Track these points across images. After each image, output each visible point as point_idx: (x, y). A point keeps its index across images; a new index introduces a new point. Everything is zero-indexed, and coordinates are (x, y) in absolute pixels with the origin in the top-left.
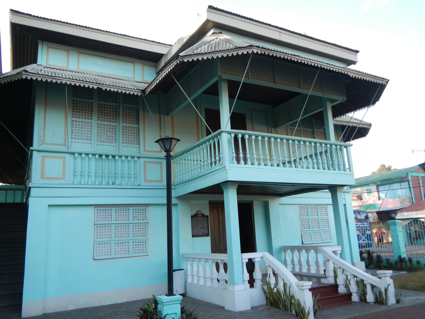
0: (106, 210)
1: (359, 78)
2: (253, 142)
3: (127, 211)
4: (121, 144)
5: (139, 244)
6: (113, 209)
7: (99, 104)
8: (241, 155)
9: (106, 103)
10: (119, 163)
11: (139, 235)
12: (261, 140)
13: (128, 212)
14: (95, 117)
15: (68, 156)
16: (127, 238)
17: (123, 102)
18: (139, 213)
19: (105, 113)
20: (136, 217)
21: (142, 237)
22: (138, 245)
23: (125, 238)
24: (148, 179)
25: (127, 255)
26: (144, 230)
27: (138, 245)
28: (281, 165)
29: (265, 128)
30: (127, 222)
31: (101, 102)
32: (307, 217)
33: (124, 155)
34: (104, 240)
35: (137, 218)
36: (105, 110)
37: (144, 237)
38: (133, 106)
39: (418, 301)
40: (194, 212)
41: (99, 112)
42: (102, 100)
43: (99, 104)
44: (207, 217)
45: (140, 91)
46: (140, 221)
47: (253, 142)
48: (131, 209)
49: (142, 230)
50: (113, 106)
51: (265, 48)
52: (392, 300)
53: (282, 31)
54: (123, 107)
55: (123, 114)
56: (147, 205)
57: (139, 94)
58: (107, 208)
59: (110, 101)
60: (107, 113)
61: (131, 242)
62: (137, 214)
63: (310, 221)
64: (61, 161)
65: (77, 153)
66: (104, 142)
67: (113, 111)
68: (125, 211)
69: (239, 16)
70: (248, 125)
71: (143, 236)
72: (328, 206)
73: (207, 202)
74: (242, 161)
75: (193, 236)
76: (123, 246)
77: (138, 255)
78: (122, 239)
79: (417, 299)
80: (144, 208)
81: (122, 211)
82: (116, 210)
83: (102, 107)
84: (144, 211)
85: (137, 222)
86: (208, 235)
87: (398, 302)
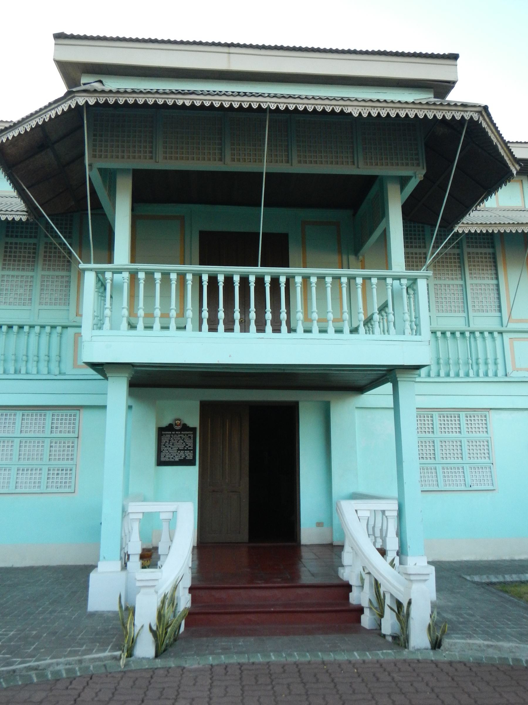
0: (6, 415)
1: (365, 115)
2: (158, 286)
3: (43, 417)
5: (60, 472)
6: (19, 413)
7: (7, 243)
8: (269, 316)
9: (19, 240)
10: (33, 338)
11: (61, 457)
12: (162, 280)
13: (44, 419)
14: (40, 267)
16: (39, 462)
17: (468, 246)
18: (64, 421)
19: (15, 257)
20: (57, 428)
21: (65, 462)
22: (58, 474)
23: (35, 462)
25: (36, 490)
26: (70, 449)
27: (58, 474)
28: (362, 329)
29: (335, 258)
30: (41, 435)
31: (9, 240)
32: (431, 435)
33: (18, 323)
34: (480, 461)
35: (59, 430)
36: (15, 252)
37: (70, 462)
38: (483, 250)
39: (490, 650)
40: (165, 423)
41: (5, 256)
42: (473, 247)
43: (7, 243)
44: (194, 429)
45: (25, 213)
46: (63, 435)
47: (158, 286)
48: (49, 414)
49: (66, 449)
50: (30, 244)
51: (126, 92)
52: (419, 639)
53: (232, 50)
54: (469, 253)
55: (45, 256)
56: (79, 408)
57: (24, 219)
58: (8, 412)
59: (26, 237)
60: (20, 257)
62: (60, 421)
63: (438, 444)
65: (486, 331)
66: (10, 304)
67: (29, 253)
68: (39, 417)
69: (318, 50)
70: (294, 254)
71: (68, 459)
72: (492, 412)
73: (198, 403)
74: (269, 328)
75: (160, 463)
76: (31, 474)
77: (55, 490)
78: (30, 462)
79: (488, 646)
80: (73, 412)
81: (34, 417)
82: (23, 415)
83: (11, 248)
84: (72, 418)
85: (59, 435)
86: (191, 463)
87: (436, 644)
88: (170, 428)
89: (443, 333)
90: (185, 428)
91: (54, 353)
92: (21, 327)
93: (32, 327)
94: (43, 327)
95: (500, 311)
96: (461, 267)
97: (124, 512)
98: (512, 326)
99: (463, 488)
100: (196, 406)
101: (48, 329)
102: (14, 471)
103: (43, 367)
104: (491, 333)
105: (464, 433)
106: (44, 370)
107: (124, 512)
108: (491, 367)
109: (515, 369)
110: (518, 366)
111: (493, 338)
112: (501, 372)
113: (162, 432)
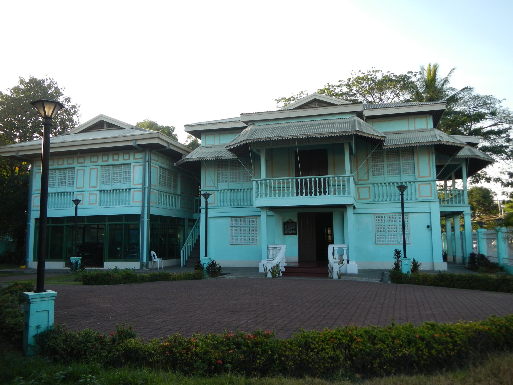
4: (402, 175)
15: (371, 186)
24: (368, 197)
40: (286, 221)
44: (296, 223)
48: (248, 218)
61: (387, 235)
64: (429, 186)
72: (410, 214)
75: (285, 234)
86: (295, 234)
87: (339, 278)
88: (287, 222)
89: (389, 183)
90: (293, 222)
91: (249, 198)
92: (238, 190)
93: (241, 190)
94: (244, 189)
95: (415, 173)
96: (399, 156)
97: (268, 248)
98: (419, 179)
99: (396, 243)
100: (296, 214)
101: (246, 190)
102: (239, 237)
103: (245, 202)
104: (381, 184)
105: (386, 222)
106: (246, 204)
107: (268, 248)
108: (385, 197)
109: (420, 196)
110: (421, 195)
111: (379, 186)
112: (414, 198)
113: (285, 224)
